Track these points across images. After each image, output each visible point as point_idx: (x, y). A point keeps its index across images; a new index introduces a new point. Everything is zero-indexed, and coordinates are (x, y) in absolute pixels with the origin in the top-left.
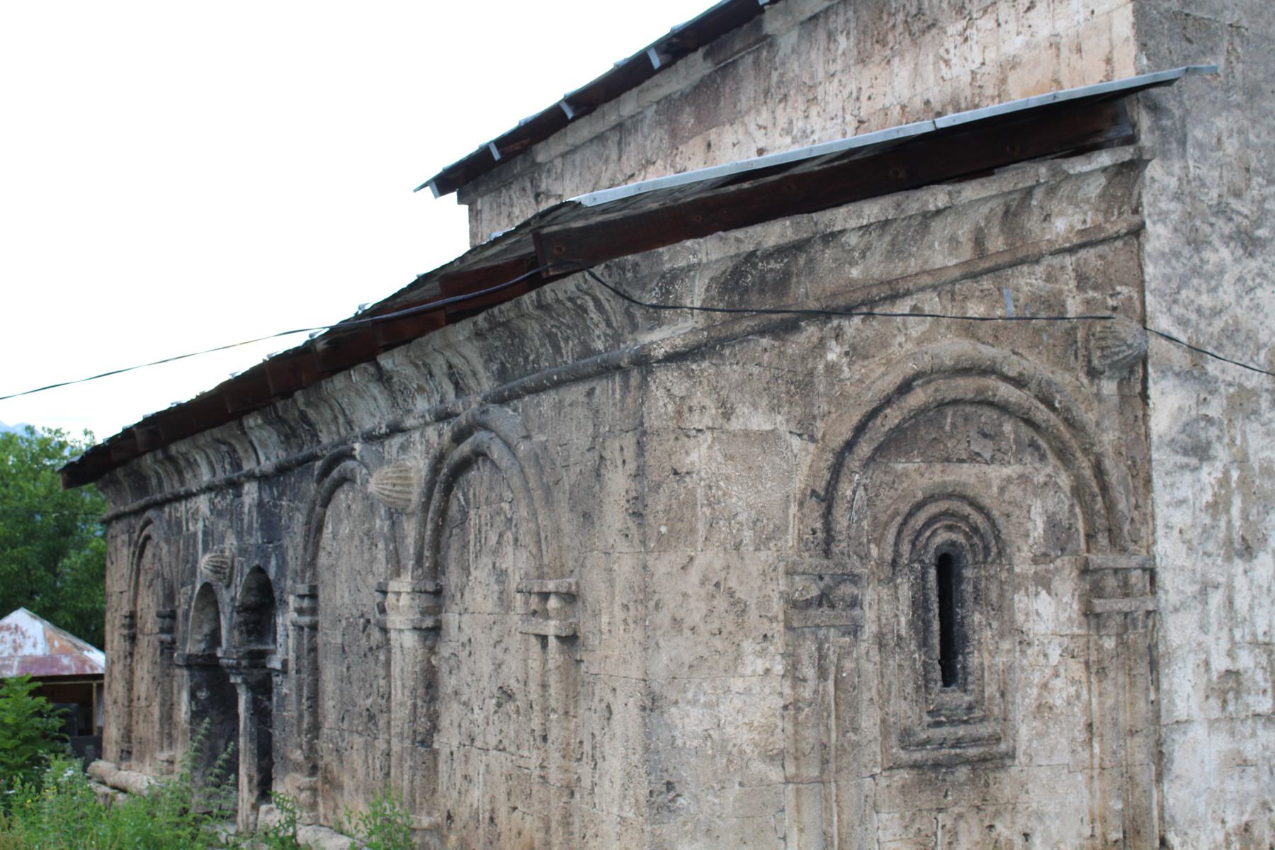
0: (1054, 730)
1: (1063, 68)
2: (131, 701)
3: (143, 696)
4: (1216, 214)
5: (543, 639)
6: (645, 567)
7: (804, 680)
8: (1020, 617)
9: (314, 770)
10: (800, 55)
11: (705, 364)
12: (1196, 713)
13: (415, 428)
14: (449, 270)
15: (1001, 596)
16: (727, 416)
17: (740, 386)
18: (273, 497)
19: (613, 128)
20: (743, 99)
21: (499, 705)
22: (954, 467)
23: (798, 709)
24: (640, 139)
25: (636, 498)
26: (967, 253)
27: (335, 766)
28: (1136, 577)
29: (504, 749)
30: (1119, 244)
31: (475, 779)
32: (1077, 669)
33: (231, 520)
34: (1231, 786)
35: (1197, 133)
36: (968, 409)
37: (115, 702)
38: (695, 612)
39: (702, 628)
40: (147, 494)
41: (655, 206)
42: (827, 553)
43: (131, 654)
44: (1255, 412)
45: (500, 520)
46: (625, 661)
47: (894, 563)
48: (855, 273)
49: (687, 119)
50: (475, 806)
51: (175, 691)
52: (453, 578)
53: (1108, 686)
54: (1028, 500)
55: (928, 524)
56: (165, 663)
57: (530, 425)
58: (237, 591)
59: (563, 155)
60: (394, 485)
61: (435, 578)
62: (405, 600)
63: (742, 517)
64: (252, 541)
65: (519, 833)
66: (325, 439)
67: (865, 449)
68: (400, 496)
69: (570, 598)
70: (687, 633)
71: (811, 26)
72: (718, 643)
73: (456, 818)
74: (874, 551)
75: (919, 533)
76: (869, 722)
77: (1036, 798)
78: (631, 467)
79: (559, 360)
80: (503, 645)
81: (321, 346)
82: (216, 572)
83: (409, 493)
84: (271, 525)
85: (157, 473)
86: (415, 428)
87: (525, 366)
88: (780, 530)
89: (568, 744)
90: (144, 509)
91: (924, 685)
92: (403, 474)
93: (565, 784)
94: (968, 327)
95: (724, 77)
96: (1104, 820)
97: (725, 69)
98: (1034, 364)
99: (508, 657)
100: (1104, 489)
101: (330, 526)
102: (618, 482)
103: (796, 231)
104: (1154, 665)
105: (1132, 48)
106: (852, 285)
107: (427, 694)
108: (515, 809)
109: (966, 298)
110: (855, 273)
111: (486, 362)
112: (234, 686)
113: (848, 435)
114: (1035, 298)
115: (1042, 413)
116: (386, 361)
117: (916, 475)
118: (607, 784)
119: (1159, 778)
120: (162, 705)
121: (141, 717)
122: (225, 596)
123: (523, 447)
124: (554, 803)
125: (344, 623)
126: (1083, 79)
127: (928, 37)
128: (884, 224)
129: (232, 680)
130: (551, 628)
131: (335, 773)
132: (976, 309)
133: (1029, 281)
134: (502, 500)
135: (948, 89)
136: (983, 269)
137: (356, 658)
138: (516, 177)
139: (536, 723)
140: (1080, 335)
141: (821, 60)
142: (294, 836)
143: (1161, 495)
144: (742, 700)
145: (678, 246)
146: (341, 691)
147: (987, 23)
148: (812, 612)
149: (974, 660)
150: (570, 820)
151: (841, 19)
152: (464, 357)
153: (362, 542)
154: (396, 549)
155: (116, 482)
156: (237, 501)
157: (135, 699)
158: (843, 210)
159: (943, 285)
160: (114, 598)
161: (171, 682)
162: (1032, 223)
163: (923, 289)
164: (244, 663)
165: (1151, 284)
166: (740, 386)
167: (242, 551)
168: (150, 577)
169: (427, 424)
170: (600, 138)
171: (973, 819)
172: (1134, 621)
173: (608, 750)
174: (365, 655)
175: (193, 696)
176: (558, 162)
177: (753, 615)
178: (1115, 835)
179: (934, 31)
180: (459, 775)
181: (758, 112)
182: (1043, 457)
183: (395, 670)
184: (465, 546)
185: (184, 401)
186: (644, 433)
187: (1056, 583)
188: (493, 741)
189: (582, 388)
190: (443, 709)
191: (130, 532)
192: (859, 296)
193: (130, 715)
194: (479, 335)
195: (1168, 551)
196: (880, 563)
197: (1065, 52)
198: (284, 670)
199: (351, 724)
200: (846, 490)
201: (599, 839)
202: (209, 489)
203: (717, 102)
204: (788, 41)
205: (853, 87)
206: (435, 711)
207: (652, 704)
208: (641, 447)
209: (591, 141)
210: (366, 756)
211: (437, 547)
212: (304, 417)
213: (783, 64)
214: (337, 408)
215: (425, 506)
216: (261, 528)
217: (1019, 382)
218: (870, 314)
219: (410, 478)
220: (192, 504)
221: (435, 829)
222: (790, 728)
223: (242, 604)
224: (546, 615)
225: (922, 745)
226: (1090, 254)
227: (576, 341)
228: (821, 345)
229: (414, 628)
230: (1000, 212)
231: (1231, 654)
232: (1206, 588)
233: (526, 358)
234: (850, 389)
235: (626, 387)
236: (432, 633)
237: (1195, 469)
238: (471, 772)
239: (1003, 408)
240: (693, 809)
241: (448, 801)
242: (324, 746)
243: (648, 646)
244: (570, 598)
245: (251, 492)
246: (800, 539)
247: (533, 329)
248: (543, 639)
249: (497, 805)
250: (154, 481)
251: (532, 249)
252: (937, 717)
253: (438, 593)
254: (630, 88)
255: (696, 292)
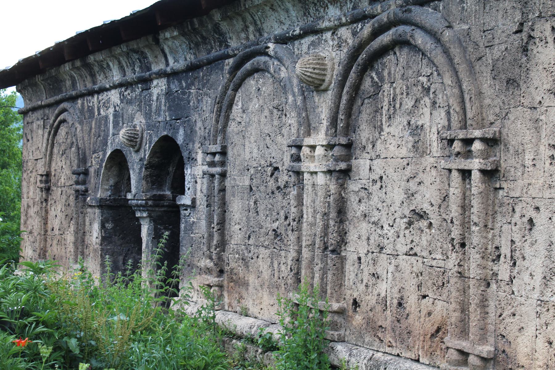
2: (46, 231)
3: (56, 227)
5: (466, 174)
13: (327, 29)
18: (182, 88)
21: (410, 223)
29: (415, 254)
31: (384, 276)
37: (31, 233)
40: (60, 91)
43: (46, 200)
45: (417, 91)
50: (383, 294)
51: (87, 223)
52: (364, 133)
56: (80, 205)
57: (451, 19)
58: (146, 151)
60: (314, 69)
61: (346, 134)
68: (317, 77)
69: (492, 142)
73: (363, 304)
80: (417, 180)
81: (66, 43)
82: (131, 141)
83: (325, 75)
84: (178, 107)
85: (72, 77)
89: (486, 249)
90: (58, 103)
92: (320, 62)
93: (483, 277)
101: (240, 104)
107: (338, 217)
112: (138, 219)
120: (76, 232)
121: (55, 242)
123: (447, 35)
125: (252, 171)
129: (138, 215)
130: (475, 164)
131: (241, 275)
134: (419, 74)
137: (263, 195)
139: (456, 233)
146: (248, 218)
150: (486, 303)
155: (34, 85)
156: (145, 93)
160: (30, 164)
161: (84, 217)
164: (150, 203)
167: (149, 127)
168: (63, 148)
173: (528, 251)
174: (273, 193)
175: (103, 226)
180: (366, 273)
183: (307, 200)
184: (377, 110)
185: (118, 17)
188: (402, 249)
191: (45, 119)
193: (46, 240)
199: (257, 240)
201: (517, 317)
202: (120, 85)
206: (343, 229)
210: (272, 263)
211: (349, 114)
216: (169, 109)
219: (326, 65)
220: (104, 96)
223: (149, 163)
224: (468, 155)
244: (492, 142)
245: (159, 87)
248: (466, 174)
249: (406, 294)
250: (68, 83)
253: (349, 146)
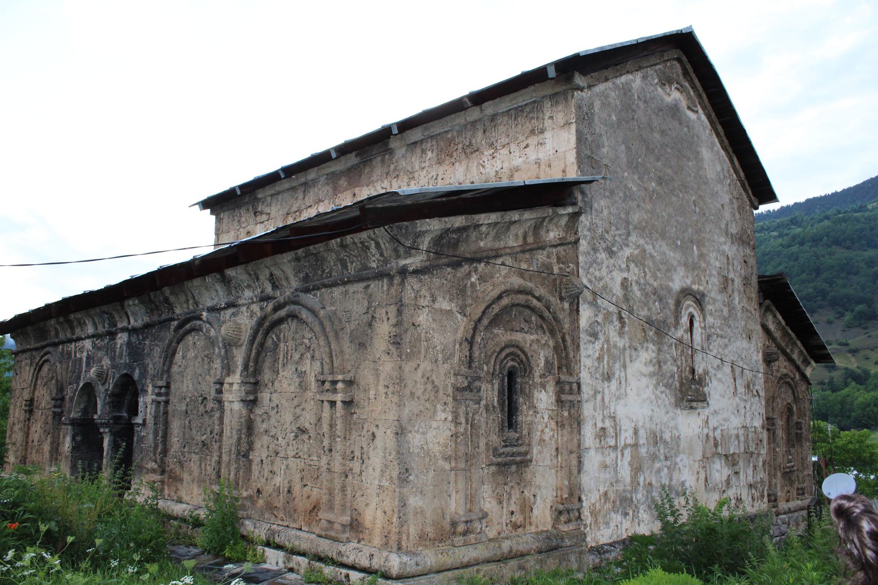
0: (545, 450)
1: (542, 172)
2: (27, 443)
3: (36, 440)
4: (601, 239)
6: (400, 368)
7: (461, 424)
8: (535, 401)
9: (163, 472)
10: (406, 158)
11: (426, 277)
12: (592, 446)
13: (243, 305)
14: (300, 225)
15: (530, 391)
16: (434, 301)
17: (439, 288)
19: (301, 185)
20: (375, 176)
21: (296, 436)
22: (514, 333)
23: (457, 437)
24: (316, 190)
25: (396, 336)
26: (520, 242)
27: (178, 470)
28: (575, 386)
30: (570, 246)
32: (553, 424)
33: (107, 351)
34: (602, 476)
35: (596, 205)
36: (521, 309)
38: (420, 389)
39: (422, 397)
40: (45, 339)
41: (409, 202)
42: (470, 367)
43: (29, 420)
44: (612, 321)
45: (302, 349)
46: (385, 412)
47: (493, 374)
48: (482, 244)
49: (343, 182)
50: (278, 485)
51: (61, 437)
52: (267, 375)
53: (565, 432)
54: (540, 351)
55: (505, 358)
59: (272, 195)
61: (254, 376)
62: (236, 387)
63: (438, 348)
64: (122, 361)
65: (309, 497)
66: (178, 311)
67: (485, 322)
69: (350, 383)
70: (416, 399)
71: (413, 147)
72: (428, 405)
74: (485, 368)
75: (502, 361)
76: (482, 443)
77: (538, 480)
78: (393, 321)
79: (345, 272)
80: (301, 407)
84: (136, 353)
86: (243, 305)
87: (322, 275)
88: (452, 355)
90: (43, 347)
91: (502, 430)
94: (521, 274)
95: (365, 166)
96: (562, 489)
97: (366, 162)
98: (541, 291)
99: (304, 413)
100: (565, 348)
102: (384, 328)
103: (466, 222)
104: (579, 424)
105: (575, 167)
106: (481, 250)
108: (305, 486)
109: (520, 261)
110: (482, 244)
111: (296, 273)
113: (480, 315)
114: (543, 264)
115: (546, 314)
116: (231, 272)
117: (502, 336)
118: (370, 470)
119: (579, 472)
120: (52, 443)
121: (34, 451)
122: (101, 389)
124: (336, 481)
125: (188, 400)
126: (554, 175)
127: (474, 155)
128: (496, 224)
129: (102, 430)
130: (339, 398)
132: (524, 266)
133: (541, 256)
134: (303, 337)
135: (483, 177)
136: (527, 249)
138: (244, 204)
139: (326, 443)
140: (558, 282)
141: (418, 161)
142: (157, 504)
143: (583, 352)
144: (435, 433)
145: (423, 221)
146: (184, 433)
147: (505, 151)
148: (464, 393)
149: (520, 418)
151: (429, 145)
152: (283, 271)
153: (203, 360)
154: (228, 363)
156: (112, 342)
157: (30, 442)
158: (483, 215)
159: (513, 255)
162: (543, 232)
163: (506, 255)
164: (111, 422)
165: (581, 265)
166: (439, 288)
169: (253, 303)
170: (293, 189)
171: (516, 487)
172: (574, 405)
173: (371, 454)
175: (73, 439)
176: (269, 199)
177: (441, 393)
178: (566, 496)
179: (477, 153)
180: (266, 470)
181: (382, 182)
182: (544, 333)
183: (226, 420)
184: (276, 360)
186: (402, 305)
187: (547, 387)
188: (291, 453)
189: (362, 285)
190: (256, 439)
192: (485, 254)
193: (26, 450)
194: (297, 259)
195: (585, 376)
196: (488, 373)
197: (543, 167)
198: (144, 424)
200: (478, 339)
203: (360, 176)
204: (400, 152)
205: (434, 174)
207: (400, 432)
208: (400, 312)
209: (288, 190)
210: (201, 464)
211: (256, 362)
212: (166, 300)
213: (397, 162)
214: (190, 295)
215: (252, 342)
217: (539, 299)
218: (488, 263)
221: (250, 498)
222: (453, 445)
223: (112, 393)
224: (335, 391)
225: (500, 455)
226: (561, 249)
227: (358, 263)
228: (469, 275)
229: (242, 400)
230: (533, 225)
231: (603, 421)
232: (596, 392)
233: (323, 271)
234: (480, 295)
235: (391, 284)
236: (251, 403)
237: (593, 343)
238: (275, 469)
239: (533, 309)
240: (416, 482)
241: (255, 485)
242: (171, 461)
243: (400, 405)
244: (350, 383)
245: (122, 339)
246: (460, 360)
247: (331, 258)
248: (333, 404)
249: (293, 484)
251: (358, 213)
252: (507, 443)
253: (256, 383)
254: (313, 167)
255: (425, 243)
